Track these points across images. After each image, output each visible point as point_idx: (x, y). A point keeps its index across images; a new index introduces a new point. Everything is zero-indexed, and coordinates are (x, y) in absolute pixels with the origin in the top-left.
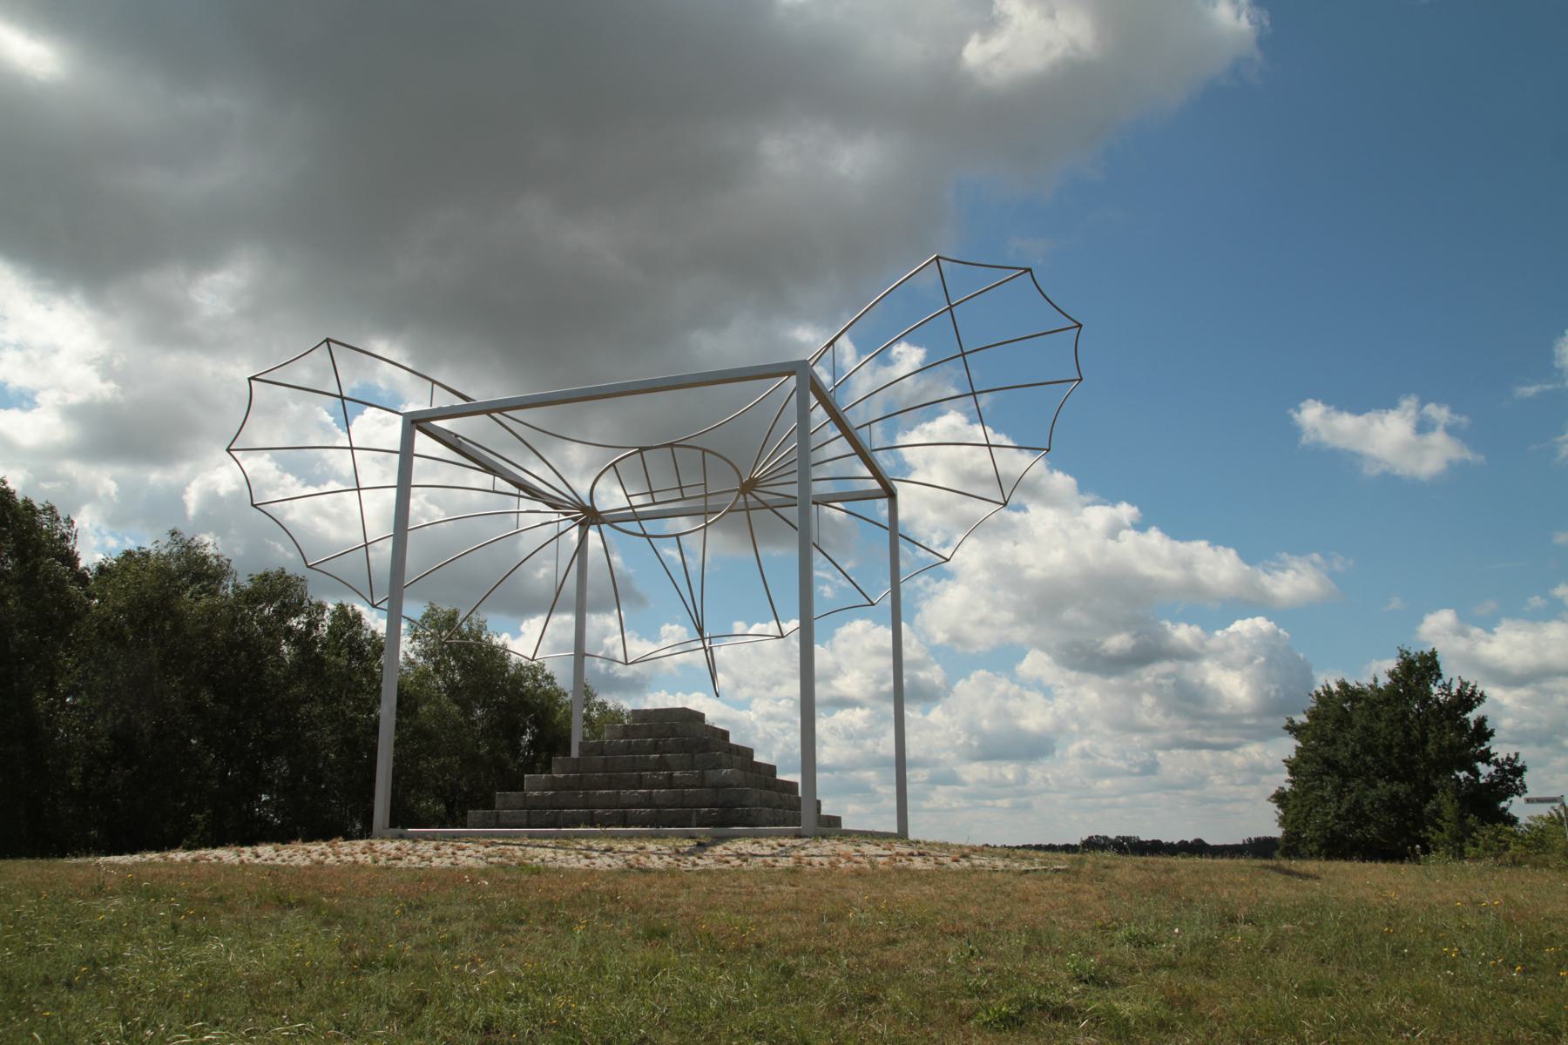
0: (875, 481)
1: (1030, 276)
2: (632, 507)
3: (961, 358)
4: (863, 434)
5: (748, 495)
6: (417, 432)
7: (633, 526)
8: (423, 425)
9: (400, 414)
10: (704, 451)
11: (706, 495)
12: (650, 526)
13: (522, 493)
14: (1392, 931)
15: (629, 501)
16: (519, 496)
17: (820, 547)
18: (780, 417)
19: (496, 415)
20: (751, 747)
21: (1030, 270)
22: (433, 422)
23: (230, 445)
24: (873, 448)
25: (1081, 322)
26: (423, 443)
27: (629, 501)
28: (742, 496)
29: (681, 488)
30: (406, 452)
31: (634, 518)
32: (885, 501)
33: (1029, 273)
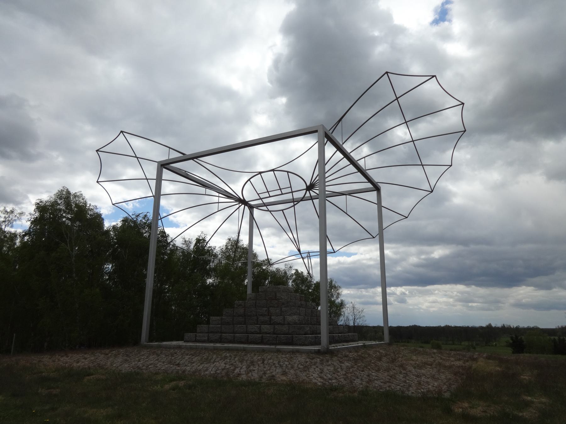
0: (369, 184)
1: (436, 79)
2: (261, 199)
3: (407, 121)
4: (361, 163)
5: (311, 191)
6: (164, 169)
7: (265, 208)
8: (167, 166)
9: (157, 162)
10: (288, 172)
11: (292, 192)
12: (270, 208)
13: (220, 195)
14: (170, 307)
15: (259, 196)
16: (219, 197)
17: (348, 213)
18: (417, 148)
19: (195, 160)
20: (487, 324)
21: (435, 76)
22: (171, 165)
23: (449, 167)
24: (366, 169)
25: (464, 102)
26: (167, 174)
27: (259, 196)
28: (308, 192)
29: (280, 189)
30: (159, 180)
31: (264, 205)
32: (376, 192)
33: (435, 77)
